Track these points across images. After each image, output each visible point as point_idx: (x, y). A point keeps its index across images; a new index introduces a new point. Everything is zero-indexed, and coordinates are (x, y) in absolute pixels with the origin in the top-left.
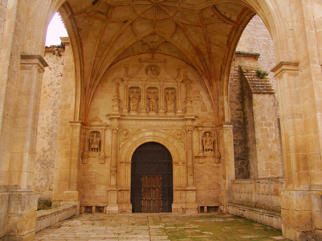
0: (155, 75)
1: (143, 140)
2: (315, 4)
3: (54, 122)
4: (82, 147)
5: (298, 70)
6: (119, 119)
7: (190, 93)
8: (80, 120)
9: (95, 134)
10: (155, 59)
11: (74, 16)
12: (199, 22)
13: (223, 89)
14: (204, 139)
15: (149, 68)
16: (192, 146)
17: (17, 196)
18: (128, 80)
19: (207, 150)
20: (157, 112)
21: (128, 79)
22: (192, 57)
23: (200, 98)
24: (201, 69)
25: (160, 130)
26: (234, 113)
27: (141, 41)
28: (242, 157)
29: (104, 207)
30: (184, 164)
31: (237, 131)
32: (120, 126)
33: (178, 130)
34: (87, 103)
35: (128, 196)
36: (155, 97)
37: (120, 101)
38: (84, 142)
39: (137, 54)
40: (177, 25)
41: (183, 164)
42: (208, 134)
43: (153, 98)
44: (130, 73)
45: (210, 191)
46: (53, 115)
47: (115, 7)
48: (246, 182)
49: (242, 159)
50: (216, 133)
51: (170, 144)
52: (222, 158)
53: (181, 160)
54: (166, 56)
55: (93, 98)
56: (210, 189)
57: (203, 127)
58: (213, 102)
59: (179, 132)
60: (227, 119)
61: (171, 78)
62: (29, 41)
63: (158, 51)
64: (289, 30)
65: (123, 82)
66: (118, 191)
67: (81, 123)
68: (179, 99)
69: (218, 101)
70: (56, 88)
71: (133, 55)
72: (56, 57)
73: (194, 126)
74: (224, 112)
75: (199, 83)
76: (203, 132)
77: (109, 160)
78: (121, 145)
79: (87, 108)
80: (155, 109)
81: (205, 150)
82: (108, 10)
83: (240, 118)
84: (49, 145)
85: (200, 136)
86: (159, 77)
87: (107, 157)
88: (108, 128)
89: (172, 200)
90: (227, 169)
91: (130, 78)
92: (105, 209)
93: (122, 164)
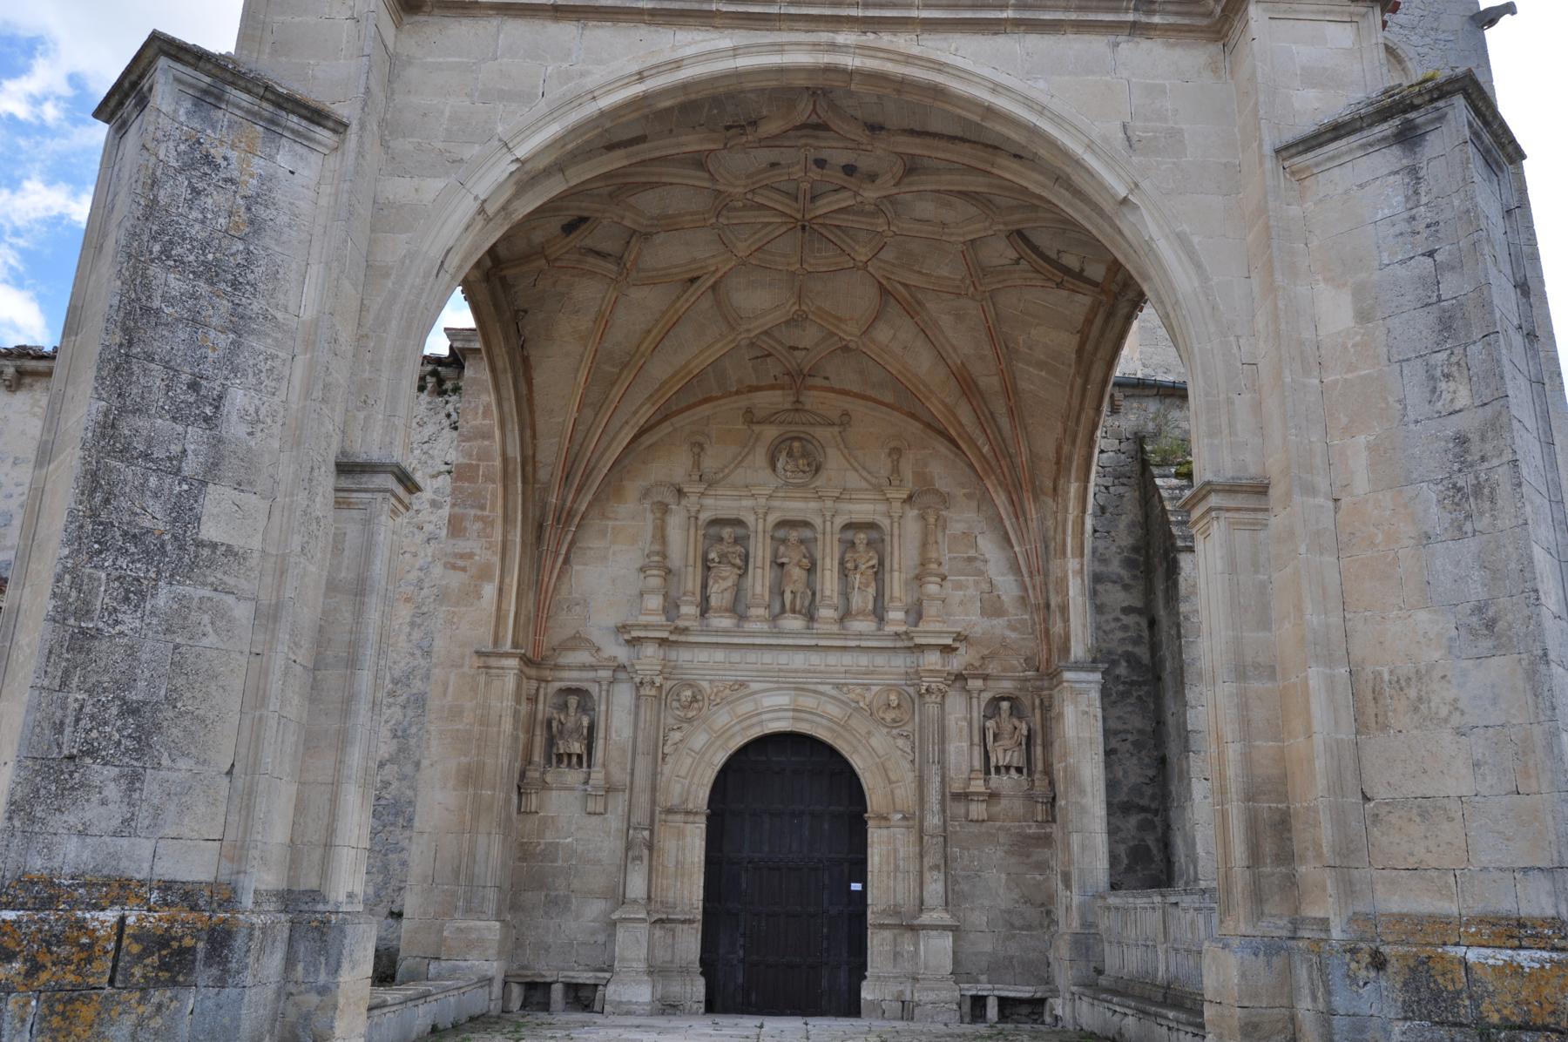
0: (804, 472)
1: (753, 725)
2: (1322, 285)
3: (418, 653)
4: (521, 747)
5: (1266, 510)
6: (663, 642)
7: (936, 542)
8: (515, 645)
9: (573, 701)
10: (806, 411)
11: (502, 270)
12: (968, 282)
13: (1064, 532)
14: (990, 724)
15: (783, 446)
16: (942, 751)
17: (314, 924)
18: (702, 494)
19: (1003, 770)
20: (811, 617)
21: (701, 488)
22: (945, 405)
23: (978, 564)
24: (981, 452)
25: (821, 688)
26: (1113, 625)
27: (752, 345)
28: (1142, 802)
29: (596, 986)
30: (911, 823)
31: (1124, 695)
32: (667, 670)
33: (890, 688)
34: (546, 579)
35: (690, 944)
36: (805, 557)
37: (669, 572)
38: (530, 731)
39: (737, 393)
40: (884, 292)
41: (905, 823)
42: (1005, 705)
43: (795, 561)
44: (709, 463)
45: (1014, 936)
46: (412, 624)
47: (651, 234)
48: (1138, 901)
49: (1143, 809)
50: (1037, 702)
51: (860, 741)
52: (1061, 803)
53: (899, 807)
54: (849, 399)
55: (566, 561)
56: (1013, 926)
57: (986, 678)
58: (1027, 579)
59: (893, 697)
60: (1078, 650)
61: (864, 485)
62: (361, 415)
63: (818, 381)
64: (1239, 365)
65: (684, 502)
66: (655, 922)
67: (521, 659)
68: (896, 566)
69: (1046, 575)
70: (427, 519)
71: (722, 397)
72: (429, 399)
73: (949, 674)
74: (1066, 620)
75: (974, 504)
76: (987, 696)
77: (619, 803)
78: (669, 742)
79: (545, 598)
80: (803, 606)
81: (993, 770)
82: (628, 243)
83: (1137, 641)
84: (395, 741)
85: (975, 714)
86: (820, 481)
87: (616, 790)
88: (622, 675)
89: (864, 966)
90: (1076, 848)
91: (710, 485)
92: (599, 995)
93: (670, 817)
